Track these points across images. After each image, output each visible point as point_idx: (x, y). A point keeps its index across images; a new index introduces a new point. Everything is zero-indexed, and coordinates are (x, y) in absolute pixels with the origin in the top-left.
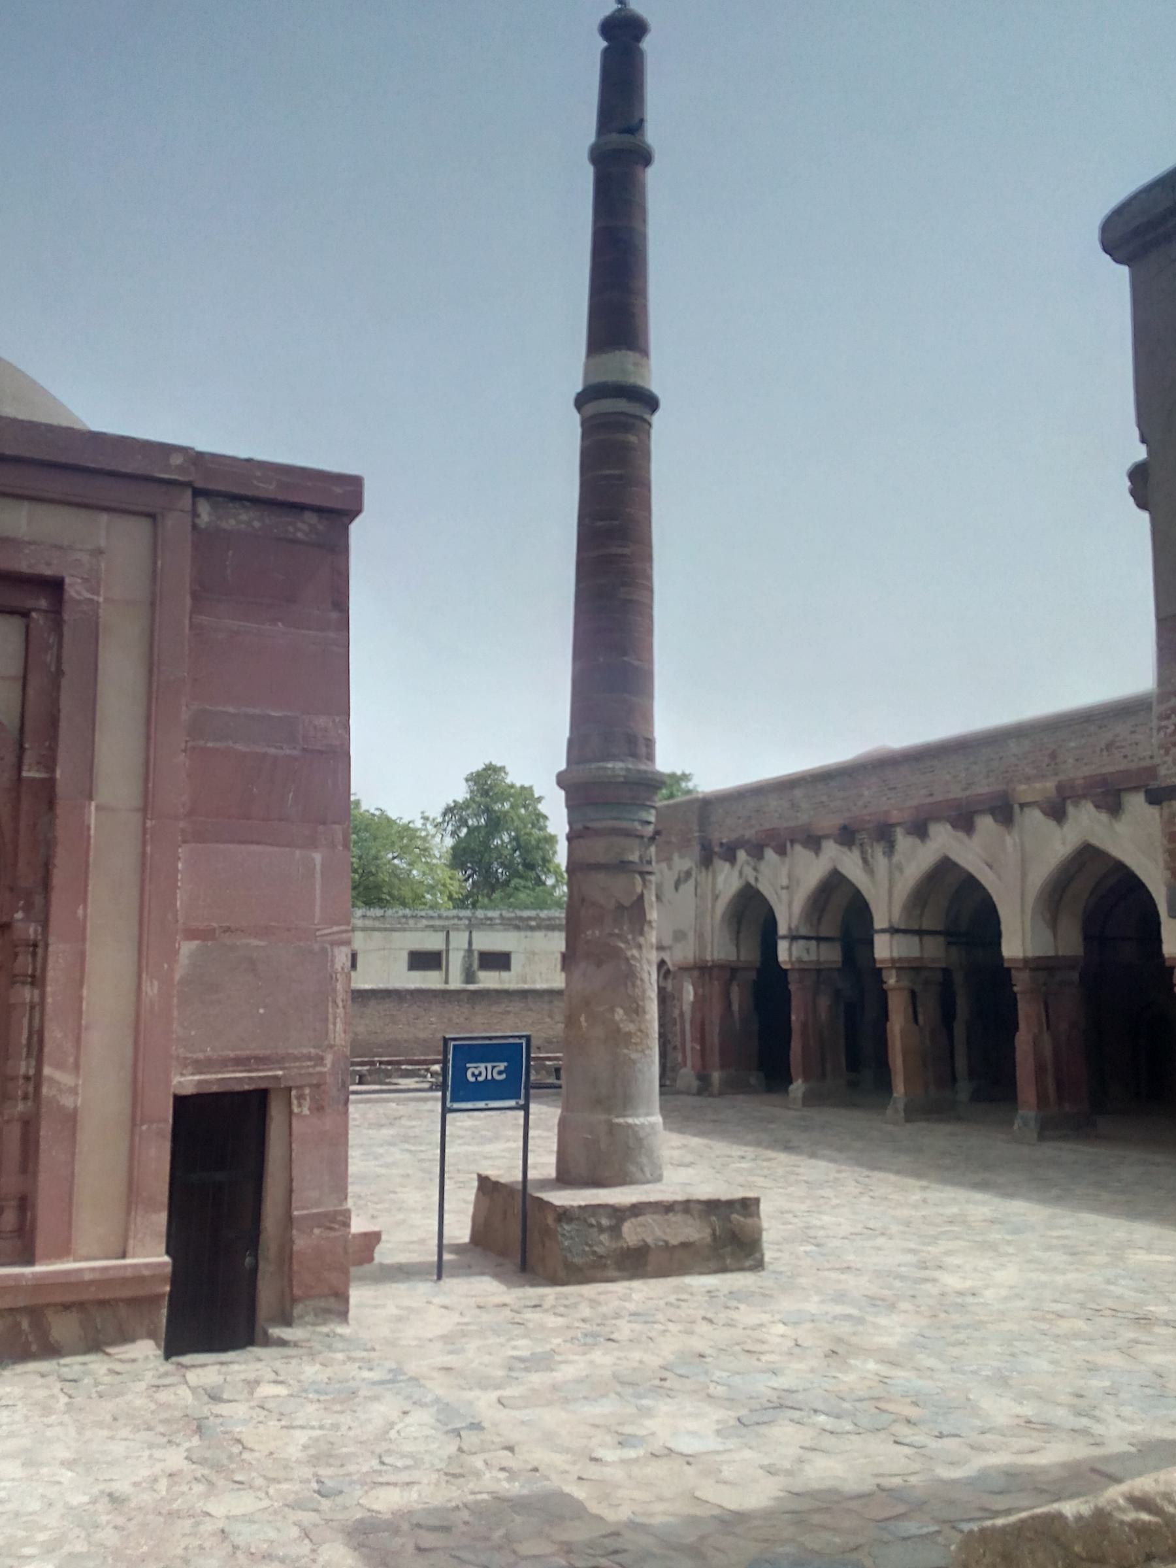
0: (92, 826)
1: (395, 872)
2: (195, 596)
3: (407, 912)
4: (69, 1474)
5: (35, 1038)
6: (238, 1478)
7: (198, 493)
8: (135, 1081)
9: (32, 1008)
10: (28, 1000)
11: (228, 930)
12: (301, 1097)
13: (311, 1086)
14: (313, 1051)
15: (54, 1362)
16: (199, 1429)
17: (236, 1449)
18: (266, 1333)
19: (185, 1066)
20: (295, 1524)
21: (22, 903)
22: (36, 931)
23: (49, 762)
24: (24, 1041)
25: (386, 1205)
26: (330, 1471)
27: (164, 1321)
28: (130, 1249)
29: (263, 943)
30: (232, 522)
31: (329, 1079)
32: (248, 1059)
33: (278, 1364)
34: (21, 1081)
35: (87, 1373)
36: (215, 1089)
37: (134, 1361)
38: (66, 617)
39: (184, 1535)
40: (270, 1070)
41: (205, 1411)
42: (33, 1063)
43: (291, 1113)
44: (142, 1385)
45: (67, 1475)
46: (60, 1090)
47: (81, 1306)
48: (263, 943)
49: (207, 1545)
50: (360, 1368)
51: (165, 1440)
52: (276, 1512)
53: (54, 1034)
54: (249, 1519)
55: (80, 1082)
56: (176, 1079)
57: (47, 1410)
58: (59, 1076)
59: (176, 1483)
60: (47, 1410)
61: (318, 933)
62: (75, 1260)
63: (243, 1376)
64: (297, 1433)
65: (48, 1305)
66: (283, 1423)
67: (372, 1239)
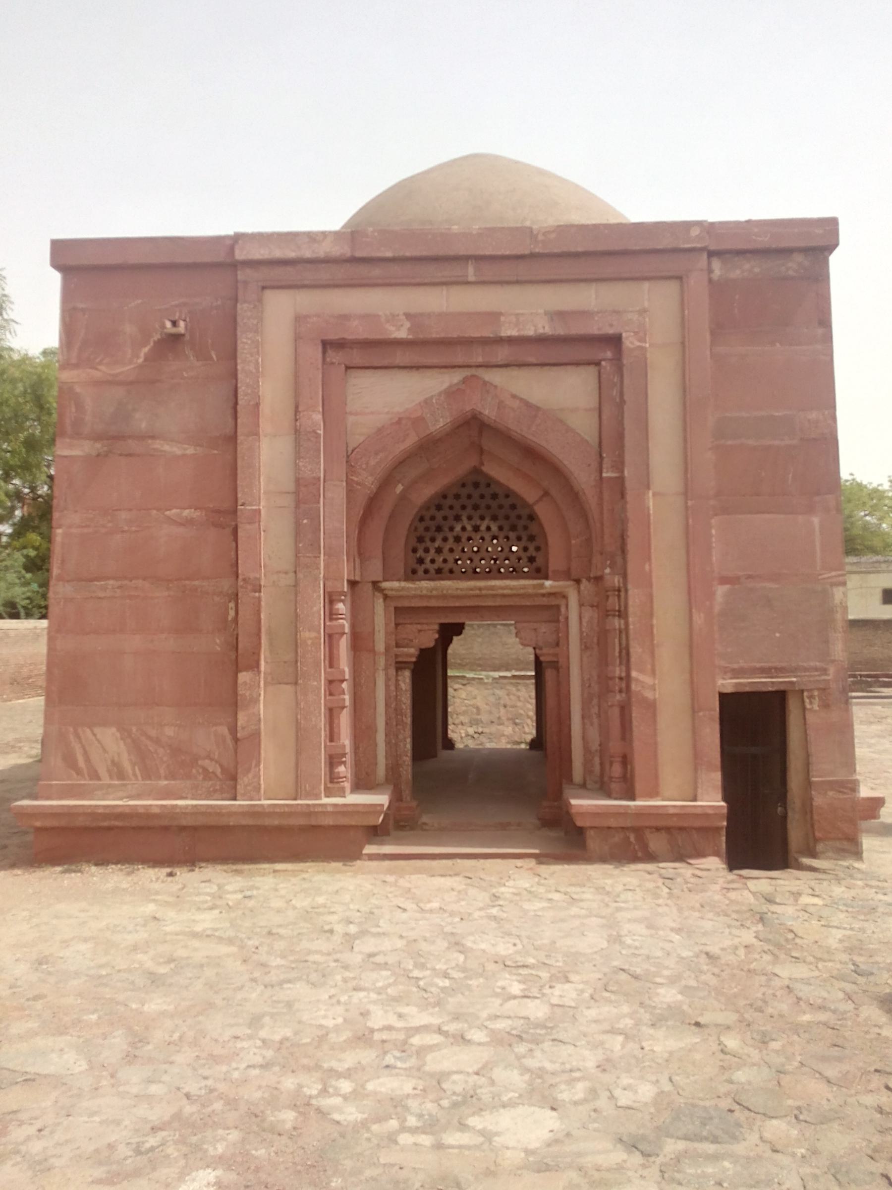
0: (651, 508)
1: (866, 527)
2: (713, 333)
3: (879, 558)
4: (678, 937)
5: (624, 651)
6: (794, 954)
7: (711, 254)
8: (692, 682)
9: (620, 632)
10: (617, 627)
11: (749, 577)
12: (811, 697)
13: (818, 689)
14: (818, 664)
15: (656, 865)
16: (762, 919)
17: (790, 936)
18: (796, 860)
19: (725, 673)
20: (840, 990)
21: (608, 562)
22: (619, 582)
23: (619, 465)
24: (617, 654)
25: (883, 781)
26: (862, 959)
27: (724, 845)
28: (699, 797)
29: (777, 586)
30: (738, 272)
31: (833, 686)
32: (770, 669)
33: (813, 883)
34: (617, 680)
35: (679, 875)
36: (748, 689)
37: (709, 870)
38: (625, 362)
39: (761, 986)
40: (788, 677)
41: (764, 908)
42: (624, 668)
43: (804, 709)
44: (717, 887)
45: (676, 938)
46: (643, 687)
47: (668, 829)
48: (777, 586)
49: (778, 993)
50: (876, 893)
51: (739, 923)
52: (825, 981)
53: (636, 650)
54: (807, 982)
55: (657, 682)
56: (720, 682)
57: (657, 896)
58: (642, 677)
59: (750, 952)
60: (657, 896)
61: (820, 577)
62: (663, 800)
63: (788, 889)
64: (834, 931)
65: (647, 827)
66: (823, 923)
67: (877, 803)
